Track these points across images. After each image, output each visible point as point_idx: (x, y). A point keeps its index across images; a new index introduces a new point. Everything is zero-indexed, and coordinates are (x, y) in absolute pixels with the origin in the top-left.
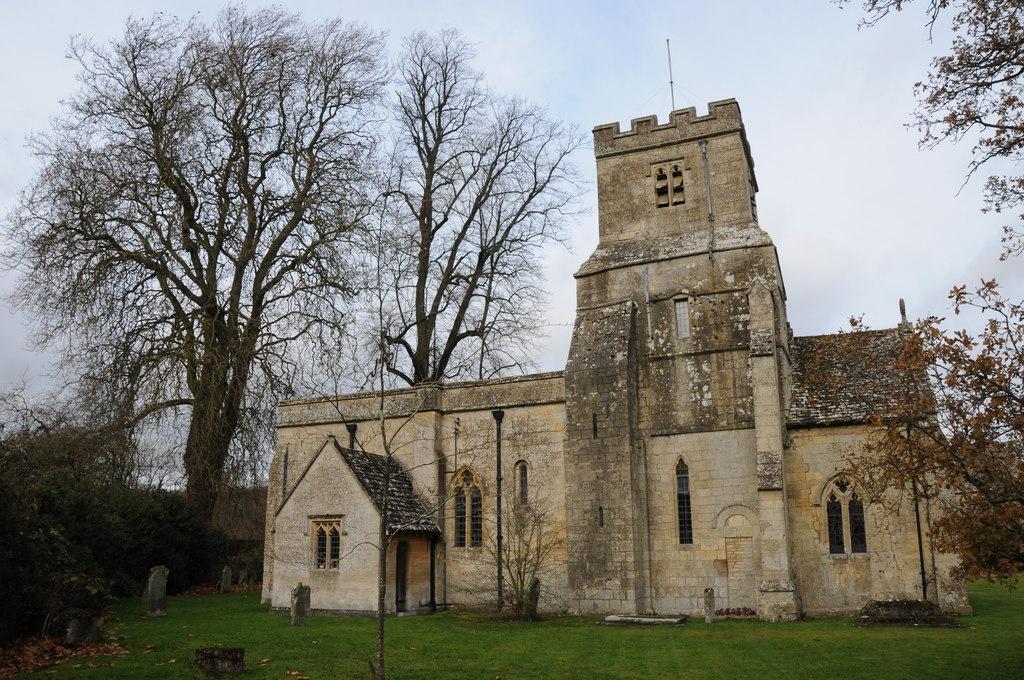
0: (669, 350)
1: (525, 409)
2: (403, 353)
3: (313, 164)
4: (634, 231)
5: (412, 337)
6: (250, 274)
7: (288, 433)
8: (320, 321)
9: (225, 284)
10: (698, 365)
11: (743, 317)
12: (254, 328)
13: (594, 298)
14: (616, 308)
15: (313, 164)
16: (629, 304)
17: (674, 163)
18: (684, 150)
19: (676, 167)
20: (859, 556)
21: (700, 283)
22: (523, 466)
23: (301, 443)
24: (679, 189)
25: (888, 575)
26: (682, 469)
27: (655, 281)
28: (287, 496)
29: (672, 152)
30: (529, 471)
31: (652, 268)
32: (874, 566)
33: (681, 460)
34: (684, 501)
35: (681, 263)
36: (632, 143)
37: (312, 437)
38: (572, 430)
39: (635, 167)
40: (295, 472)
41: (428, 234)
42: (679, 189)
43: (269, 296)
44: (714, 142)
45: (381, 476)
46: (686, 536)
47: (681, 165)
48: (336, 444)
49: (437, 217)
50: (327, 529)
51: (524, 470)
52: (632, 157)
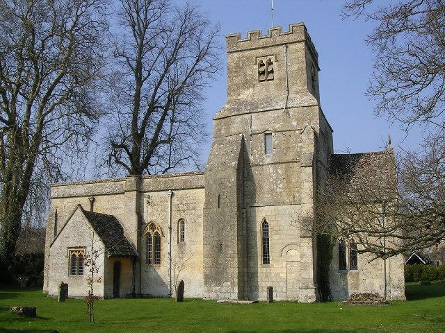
0: (261, 161)
1: (185, 191)
2: (124, 154)
3: (73, 39)
4: (246, 94)
5: (131, 145)
6: (36, 105)
7: (57, 201)
8: (77, 133)
9: (22, 111)
10: (275, 169)
11: (300, 144)
12: (38, 138)
13: (223, 132)
14: (234, 137)
15: (73, 39)
16: (241, 135)
17: (269, 57)
18: (275, 50)
19: (270, 60)
20: (354, 271)
21: (279, 125)
22: (181, 221)
23: (64, 206)
24: (272, 72)
25: (367, 281)
26: (265, 224)
27: (257, 123)
28: (56, 235)
29: (269, 51)
30: (185, 225)
31: (254, 116)
32: (361, 277)
33: (265, 221)
34: (266, 242)
35: (270, 114)
36: (246, 45)
37: (69, 204)
38: (208, 204)
39: (248, 59)
40: (61, 223)
41: (140, 81)
42: (272, 72)
43: (46, 119)
44: (291, 46)
45: (105, 226)
46: (266, 260)
47: (273, 59)
48: (82, 208)
49: (145, 74)
50: (77, 254)
51: (183, 223)
52: (246, 53)
